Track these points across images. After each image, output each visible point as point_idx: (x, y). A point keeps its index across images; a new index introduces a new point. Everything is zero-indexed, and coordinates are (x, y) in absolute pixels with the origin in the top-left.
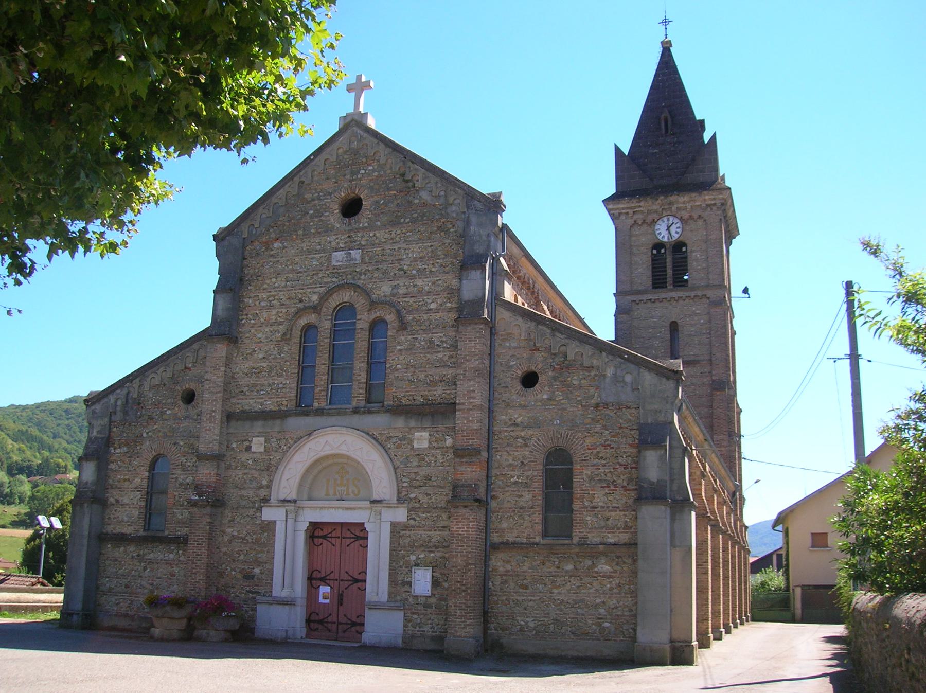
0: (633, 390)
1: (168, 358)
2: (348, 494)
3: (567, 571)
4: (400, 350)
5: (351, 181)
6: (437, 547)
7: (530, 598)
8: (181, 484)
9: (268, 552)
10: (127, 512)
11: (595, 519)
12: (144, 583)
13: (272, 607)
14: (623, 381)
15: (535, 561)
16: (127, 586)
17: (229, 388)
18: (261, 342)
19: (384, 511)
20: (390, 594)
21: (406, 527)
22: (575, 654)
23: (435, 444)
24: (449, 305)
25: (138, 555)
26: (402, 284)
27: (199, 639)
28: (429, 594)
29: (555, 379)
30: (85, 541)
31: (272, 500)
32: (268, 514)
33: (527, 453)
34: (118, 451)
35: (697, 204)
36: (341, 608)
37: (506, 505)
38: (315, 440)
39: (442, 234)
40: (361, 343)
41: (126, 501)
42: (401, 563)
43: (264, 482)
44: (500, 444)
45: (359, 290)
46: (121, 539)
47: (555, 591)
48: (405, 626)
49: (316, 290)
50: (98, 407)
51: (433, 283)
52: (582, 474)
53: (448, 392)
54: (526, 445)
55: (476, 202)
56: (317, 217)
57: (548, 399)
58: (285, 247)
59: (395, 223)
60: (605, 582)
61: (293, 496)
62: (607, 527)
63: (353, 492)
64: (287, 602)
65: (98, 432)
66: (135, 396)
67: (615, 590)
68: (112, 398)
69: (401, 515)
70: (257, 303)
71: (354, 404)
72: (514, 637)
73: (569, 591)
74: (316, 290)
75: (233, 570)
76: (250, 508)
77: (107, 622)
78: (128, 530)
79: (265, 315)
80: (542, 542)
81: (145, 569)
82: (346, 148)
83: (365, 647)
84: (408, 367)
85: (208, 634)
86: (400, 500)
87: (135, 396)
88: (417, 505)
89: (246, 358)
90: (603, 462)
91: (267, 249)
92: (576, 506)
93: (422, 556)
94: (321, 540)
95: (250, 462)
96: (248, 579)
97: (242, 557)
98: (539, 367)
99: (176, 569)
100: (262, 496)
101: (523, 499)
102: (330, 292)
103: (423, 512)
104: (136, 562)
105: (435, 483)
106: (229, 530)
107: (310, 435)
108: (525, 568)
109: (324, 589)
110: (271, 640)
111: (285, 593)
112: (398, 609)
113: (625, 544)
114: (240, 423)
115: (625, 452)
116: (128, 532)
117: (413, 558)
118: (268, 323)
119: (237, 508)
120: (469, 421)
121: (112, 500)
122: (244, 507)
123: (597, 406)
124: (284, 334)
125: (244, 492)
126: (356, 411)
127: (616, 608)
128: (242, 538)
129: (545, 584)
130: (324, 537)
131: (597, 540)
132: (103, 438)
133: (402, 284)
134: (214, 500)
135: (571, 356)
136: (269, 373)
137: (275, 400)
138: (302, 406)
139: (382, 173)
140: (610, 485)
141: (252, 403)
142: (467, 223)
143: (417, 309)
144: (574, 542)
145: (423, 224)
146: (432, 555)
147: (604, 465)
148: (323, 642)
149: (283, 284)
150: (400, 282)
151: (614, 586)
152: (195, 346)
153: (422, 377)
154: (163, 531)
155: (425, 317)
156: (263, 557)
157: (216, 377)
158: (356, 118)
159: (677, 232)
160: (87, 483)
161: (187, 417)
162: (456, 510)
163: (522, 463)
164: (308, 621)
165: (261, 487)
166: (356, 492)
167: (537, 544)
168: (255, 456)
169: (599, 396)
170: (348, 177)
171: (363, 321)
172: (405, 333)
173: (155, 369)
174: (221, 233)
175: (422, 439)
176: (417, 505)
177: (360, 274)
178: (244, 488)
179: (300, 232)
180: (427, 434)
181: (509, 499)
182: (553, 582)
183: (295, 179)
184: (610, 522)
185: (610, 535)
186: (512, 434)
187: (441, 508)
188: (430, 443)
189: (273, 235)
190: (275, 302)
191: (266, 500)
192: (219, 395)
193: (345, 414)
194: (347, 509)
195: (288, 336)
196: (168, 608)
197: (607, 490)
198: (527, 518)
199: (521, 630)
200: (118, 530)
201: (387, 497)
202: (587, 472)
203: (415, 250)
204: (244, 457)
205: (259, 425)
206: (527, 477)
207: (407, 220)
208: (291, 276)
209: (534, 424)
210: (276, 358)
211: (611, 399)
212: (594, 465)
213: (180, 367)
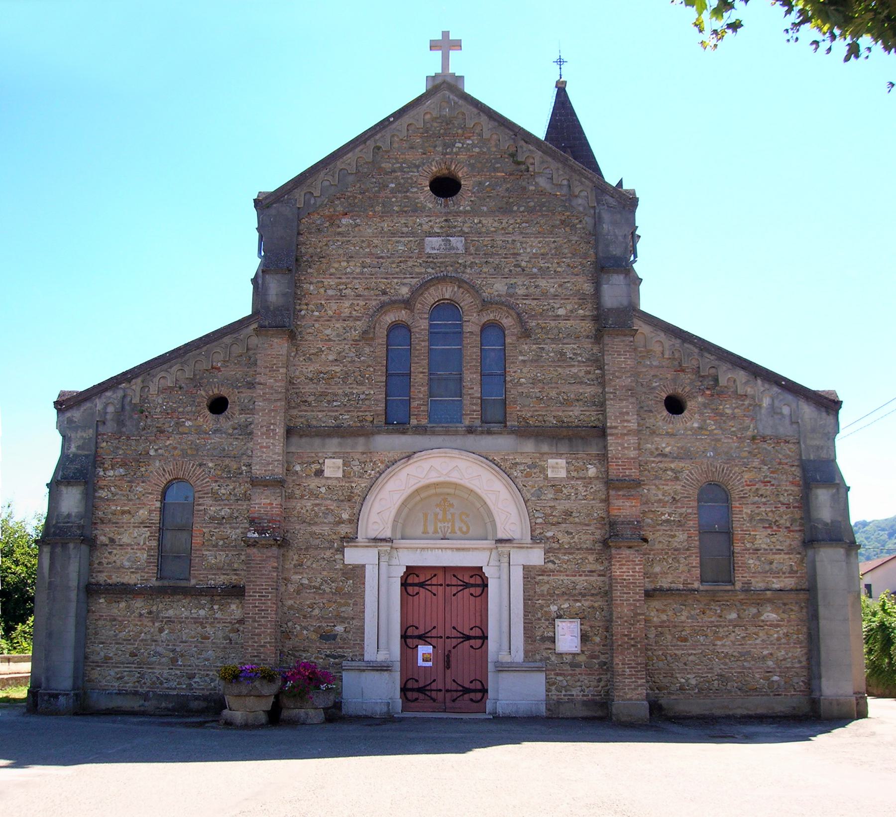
0: (792, 423)
1: (186, 353)
2: (453, 532)
3: (730, 621)
4: (524, 361)
5: (444, 154)
6: (584, 595)
7: (690, 652)
8: (212, 518)
9: (355, 604)
10: (130, 551)
11: (758, 563)
12: (159, 649)
13: (364, 674)
14: (781, 414)
15: (695, 609)
16: (133, 655)
17: (292, 396)
18: (330, 340)
20: (526, 652)
21: (543, 572)
22: (745, 712)
23: (574, 474)
24: (581, 312)
25: (150, 613)
26: (520, 283)
27: (293, 723)
28: (577, 650)
29: (705, 406)
30: (73, 595)
31: (360, 539)
32: (353, 556)
33: (680, 487)
34: (111, 473)
36: (448, 672)
37: (658, 546)
38: (416, 464)
39: (567, 229)
40: (471, 350)
41: (125, 539)
42: (539, 615)
43: (345, 516)
44: (646, 476)
45: (465, 285)
46: (124, 591)
47: (719, 643)
48: (548, 690)
49: (405, 281)
50: (76, 414)
51: (560, 286)
52: (742, 513)
53: (588, 413)
54: (677, 479)
55: (607, 197)
56: (399, 192)
57: (699, 428)
58: (357, 225)
59: (505, 210)
60: (772, 632)
61: (388, 534)
62: (771, 571)
63: (460, 529)
64: (383, 668)
65: (78, 448)
66: (136, 400)
67: (783, 641)
68: (99, 403)
69: (536, 557)
70: (322, 290)
71: (467, 422)
72: (672, 697)
73: (733, 643)
74: (405, 281)
75: (305, 628)
76: (325, 548)
77: (105, 703)
78: (131, 579)
79: (334, 307)
80: (702, 588)
81: (161, 630)
82: (435, 114)
83: (498, 719)
84: (534, 381)
85: (307, 714)
86: (536, 539)
87: (136, 400)
88: (556, 546)
89: (311, 360)
90: (764, 500)
91: (332, 224)
92: (738, 547)
93: (566, 606)
94: (416, 589)
95: (323, 490)
96: (327, 640)
97: (316, 612)
98: (687, 389)
99: (209, 630)
100: (343, 534)
101: (676, 539)
102: (425, 285)
103: (565, 554)
104: (146, 621)
105: (577, 520)
106: (296, 577)
107: (409, 457)
108: (683, 618)
109: (424, 650)
110: (366, 717)
111: (381, 657)
112: (539, 670)
113: (791, 590)
114: (304, 440)
115: (786, 490)
116: (132, 582)
117: (554, 608)
118: (338, 316)
119: (307, 549)
120: (624, 448)
121: (103, 539)
122: (317, 548)
123: (753, 438)
124: (365, 332)
126: (470, 431)
127: (785, 659)
128: (315, 587)
129: (706, 636)
130: (422, 585)
131: (761, 585)
132: (87, 456)
133: (520, 283)
134: (276, 537)
136: (345, 380)
137: (355, 414)
138: (396, 421)
139: (485, 150)
140: (771, 525)
141: (322, 417)
142: (598, 221)
143: (541, 314)
144: (737, 588)
145: (542, 216)
146: (578, 604)
147: (765, 504)
148: (418, 715)
149: (358, 270)
150: (519, 281)
151: (781, 635)
152: (227, 340)
153: (553, 394)
154: (188, 580)
155: (553, 324)
156: (348, 611)
157: (272, 381)
158: (449, 79)
160: (69, 515)
161: (216, 431)
162: (618, 551)
163: (674, 499)
164: (404, 690)
165: (341, 522)
166: (464, 529)
167: (695, 590)
168: (329, 482)
169: (756, 428)
170: (439, 149)
171: (473, 322)
172: (528, 341)
173: (165, 367)
174: (266, 198)
175: (557, 467)
176: (556, 546)
177: (465, 267)
178: (315, 524)
179: (379, 208)
180: (564, 461)
181: (661, 539)
182: (716, 632)
183: (368, 143)
184: (774, 565)
185: (775, 580)
186: (661, 465)
187: (587, 549)
188: (568, 472)
189: (340, 208)
190: (348, 291)
191: (350, 539)
192: (279, 404)
193: (456, 433)
194: (458, 549)
195: (371, 335)
196: (257, 683)
197: (769, 531)
198: (682, 560)
199: (682, 688)
200: (115, 579)
201: (517, 535)
202: (747, 510)
203: (534, 246)
204: (313, 483)
205: (333, 444)
206: (681, 514)
207: (522, 209)
208: (368, 261)
209: (685, 455)
210: (353, 362)
211: (768, 432)
212: (754, 504)
213: (205, 365)
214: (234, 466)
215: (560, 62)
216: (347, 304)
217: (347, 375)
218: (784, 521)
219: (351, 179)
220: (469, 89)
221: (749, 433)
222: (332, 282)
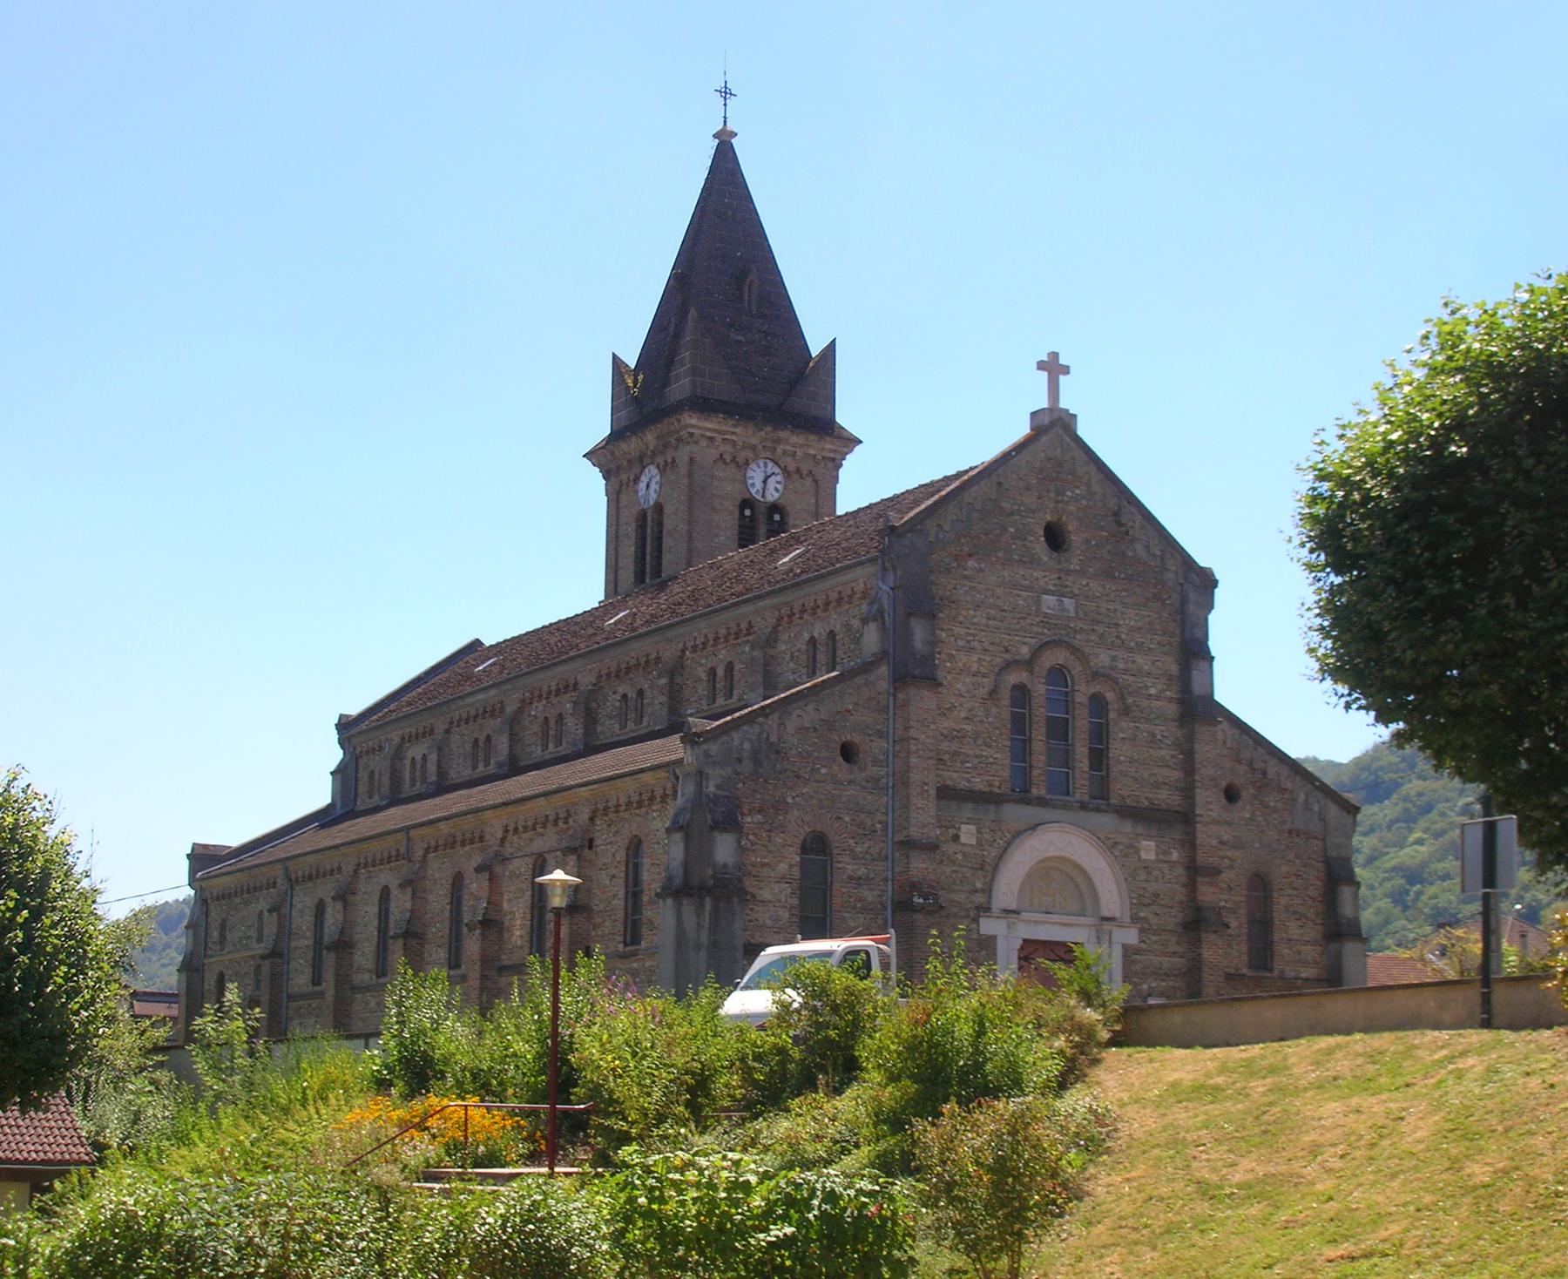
5: (1057, 502)
8: (851, 878)
19: (1115, 930)
21: (1138, 951)
35: (812, 452)
52: (1281, 902)
61: (1013, 907)
65: (718, 787)
69: (1131, 936)
84: (1131, 761)
86: (1135, 919)
92: (1276, 937)
95: (959, 856)
117: (1145, 986)
123: (1290, 832)
125: (955, 897)
126: (1083, 807)
135: (1271, 774)
138: (1021, 793)
153: (1146, 774)
155: (1146, 703)
159: (777, 490)
160: (725, 865)
161: (851, 782)
165: (975, 891)
168: (966, 849)
175: (1148, 849)
179: (1000, 554)
190: (975, 644)
191: (985, 909)
194: (1064, 924)
201: (1117, 915)
202: (1284, 901)
205: (968, 809)
214: (868, 822)
215: (726, 93)
216: (975, 657)
217: (977, 735)
218: (1311, 914)
219: (976, 515)
220: (1083, 431)
221: (1287, 827)
222: (962, 631)
